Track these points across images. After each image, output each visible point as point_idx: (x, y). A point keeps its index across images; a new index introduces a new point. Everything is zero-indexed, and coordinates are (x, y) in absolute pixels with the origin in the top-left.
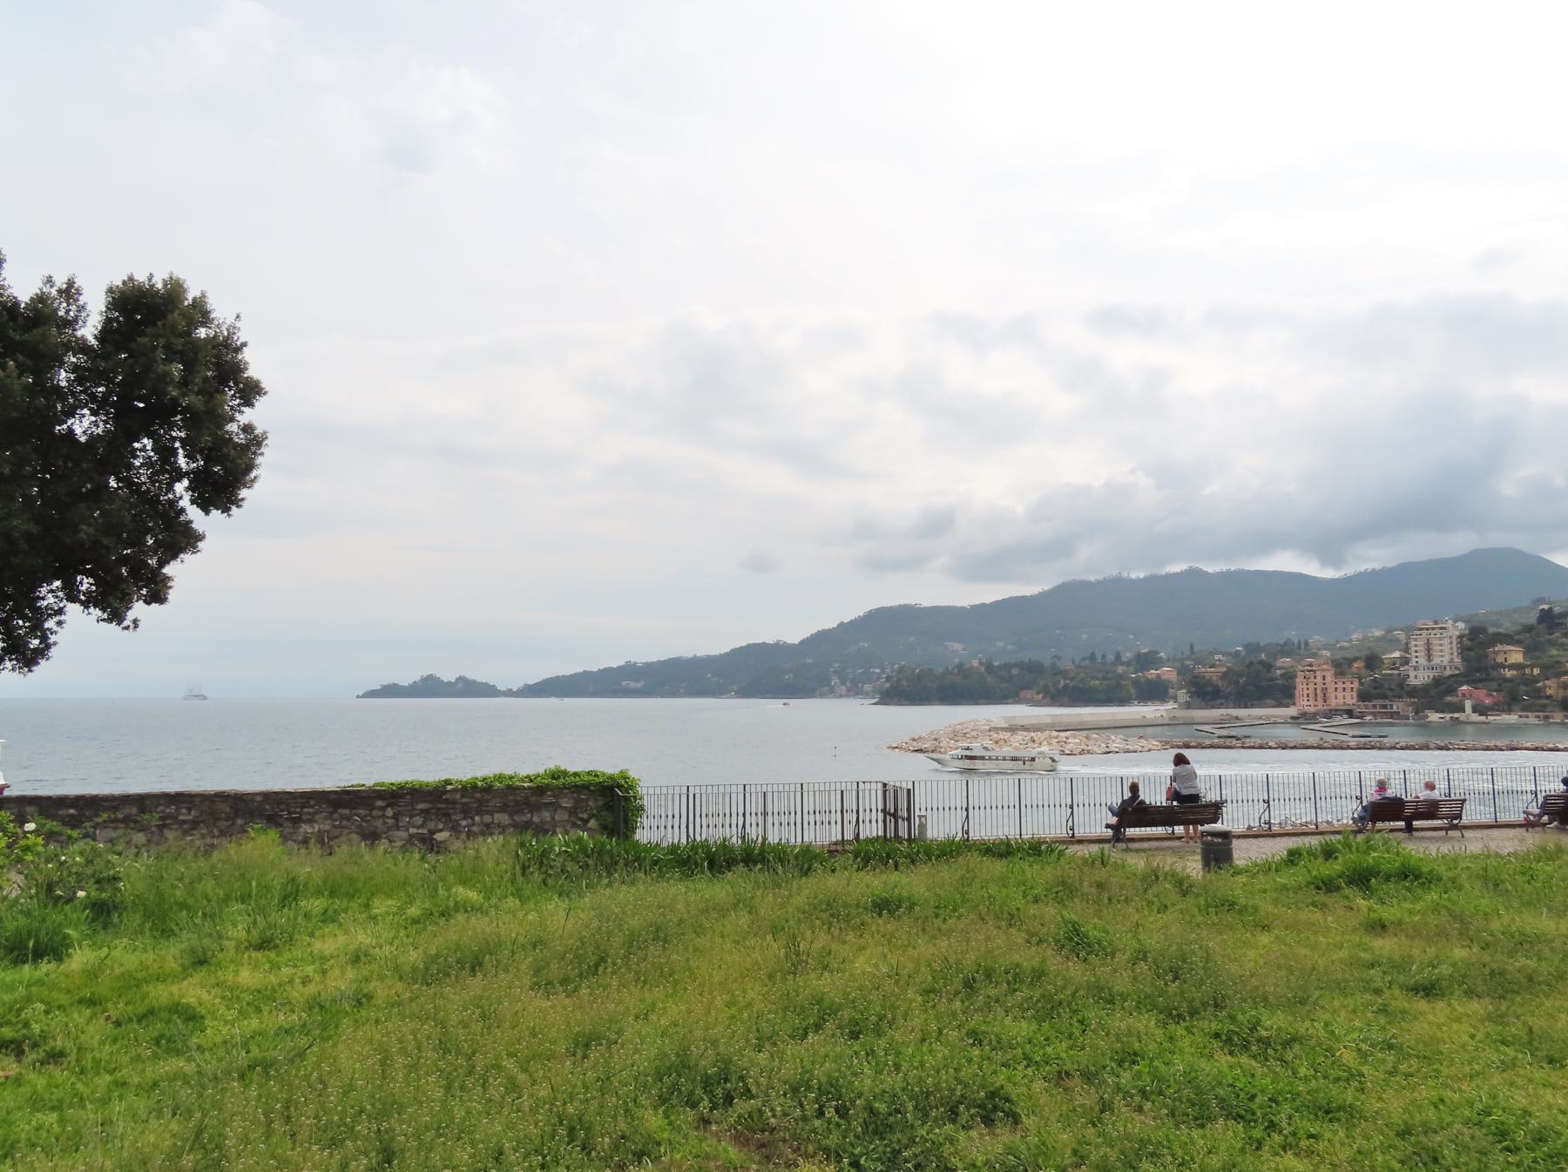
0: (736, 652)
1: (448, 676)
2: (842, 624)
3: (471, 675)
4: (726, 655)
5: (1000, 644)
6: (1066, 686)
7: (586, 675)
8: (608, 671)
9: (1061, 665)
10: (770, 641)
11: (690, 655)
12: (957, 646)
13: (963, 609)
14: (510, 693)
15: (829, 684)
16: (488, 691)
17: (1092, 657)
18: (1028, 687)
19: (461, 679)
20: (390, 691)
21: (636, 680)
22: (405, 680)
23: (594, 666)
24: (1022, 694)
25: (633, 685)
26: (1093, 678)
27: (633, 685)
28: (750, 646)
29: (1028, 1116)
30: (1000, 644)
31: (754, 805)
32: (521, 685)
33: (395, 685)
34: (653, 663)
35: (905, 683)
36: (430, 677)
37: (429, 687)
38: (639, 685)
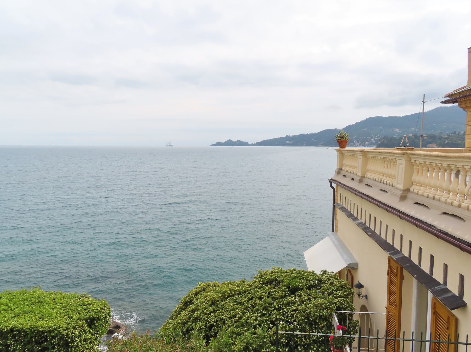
0: (322, 133)
1: (235, 140)
2: (357, 123)
3: (241, 140)
4: (318, 133)
5: (413, 129)
6: (448, 143)
7: (275, 139)
8: (281, 138)
9: (442, 135)
10: (353, 123)
11: (306, 133)
12: (397, 130)
13: (399, 117)
14: (252, 145)
15: (353, 142)
16: (246, 144)
17: (455, 133)
18: (431, 143)
19: (238, 141)
20: (219, 144)
21: (290, 141)
22: (223, 141)
23: (277, 137)
24: (428, 146)
25: (289, 142)
26: (459, 140)
27: (289, 142)
28: (326, 130)
29: (222, 315)
30: (413, 129)
31: (420, 171)
32: (255, 143)
33: (220, 142)
34: (295, 136)
35: (386, 141)
36: (230, 140)
37: (230, 143)
38: (291, 142)
